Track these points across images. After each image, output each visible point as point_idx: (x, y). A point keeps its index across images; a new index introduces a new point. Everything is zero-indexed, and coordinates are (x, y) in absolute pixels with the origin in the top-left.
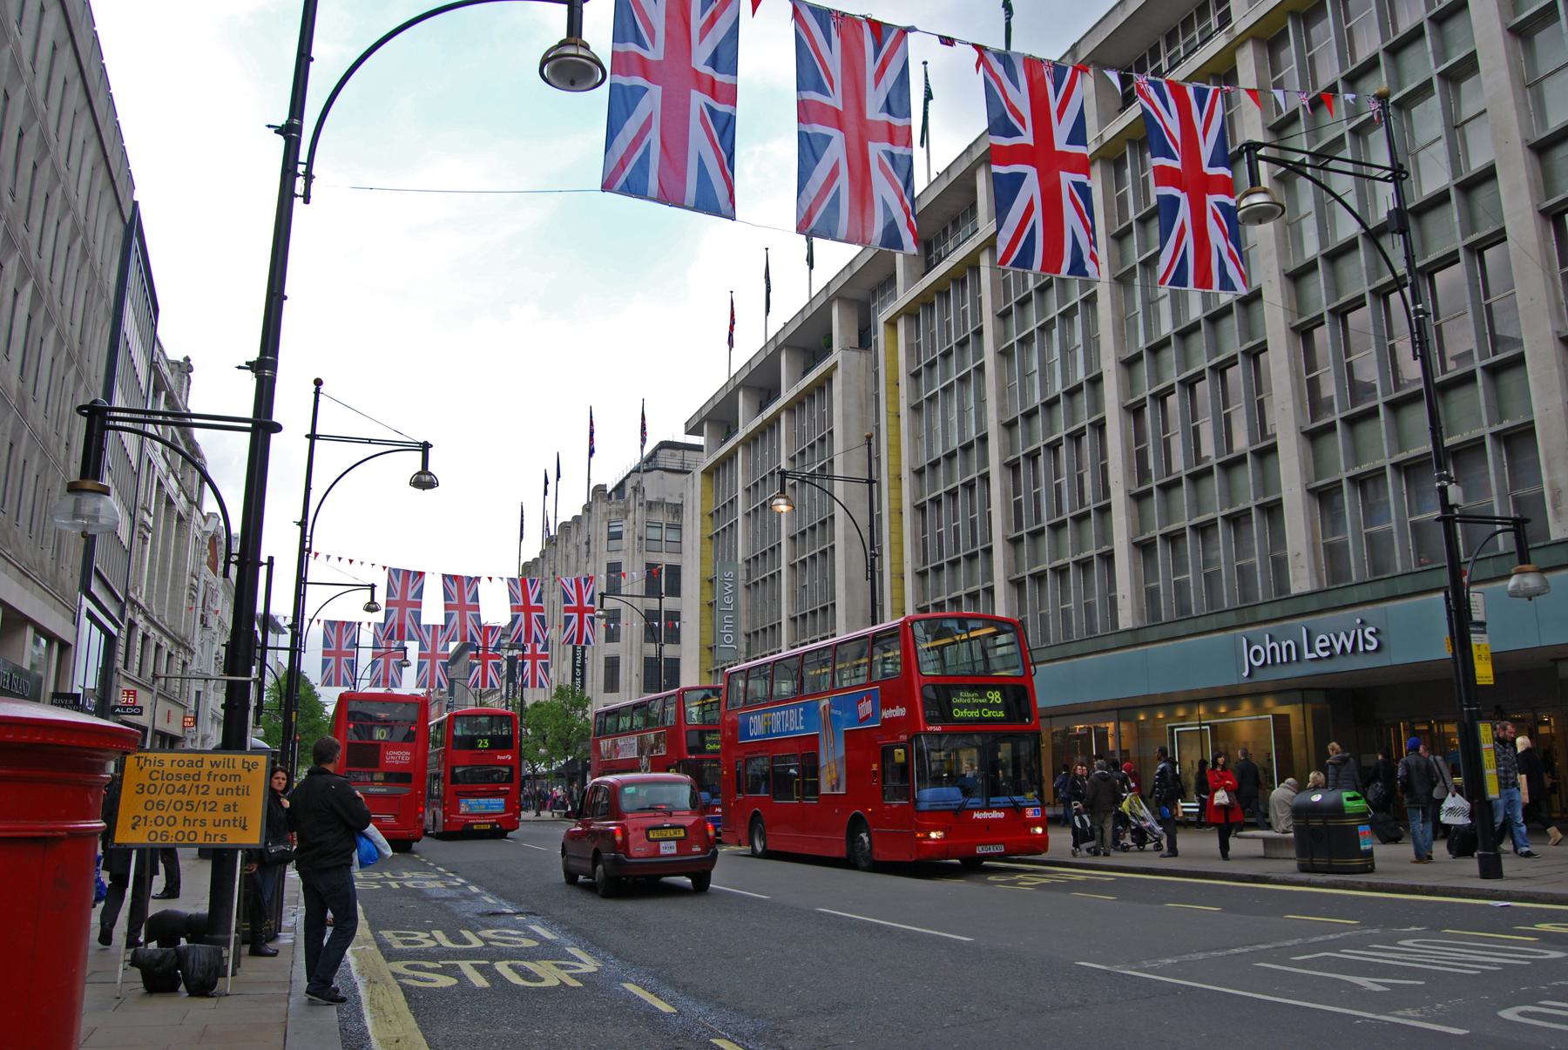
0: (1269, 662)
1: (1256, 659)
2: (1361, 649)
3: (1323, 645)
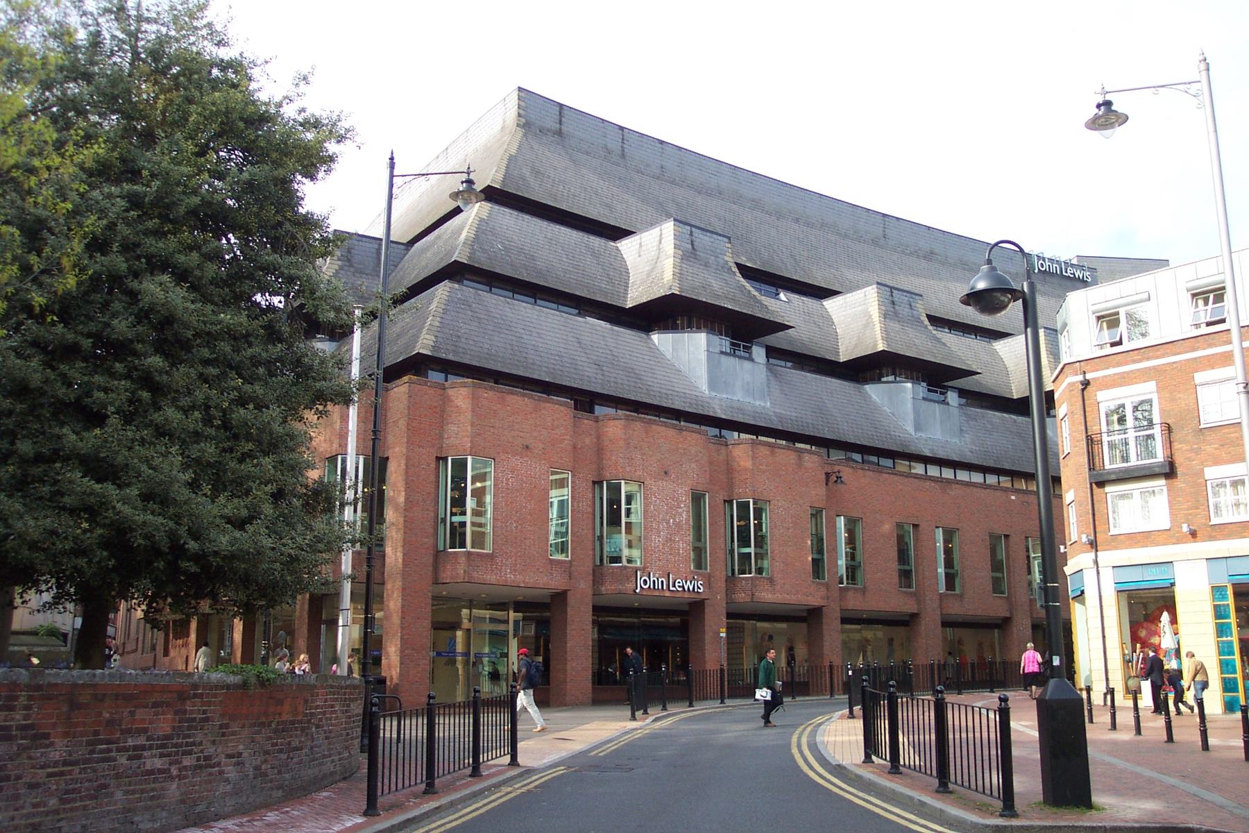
0: (652, 587)
1: (645, 581)
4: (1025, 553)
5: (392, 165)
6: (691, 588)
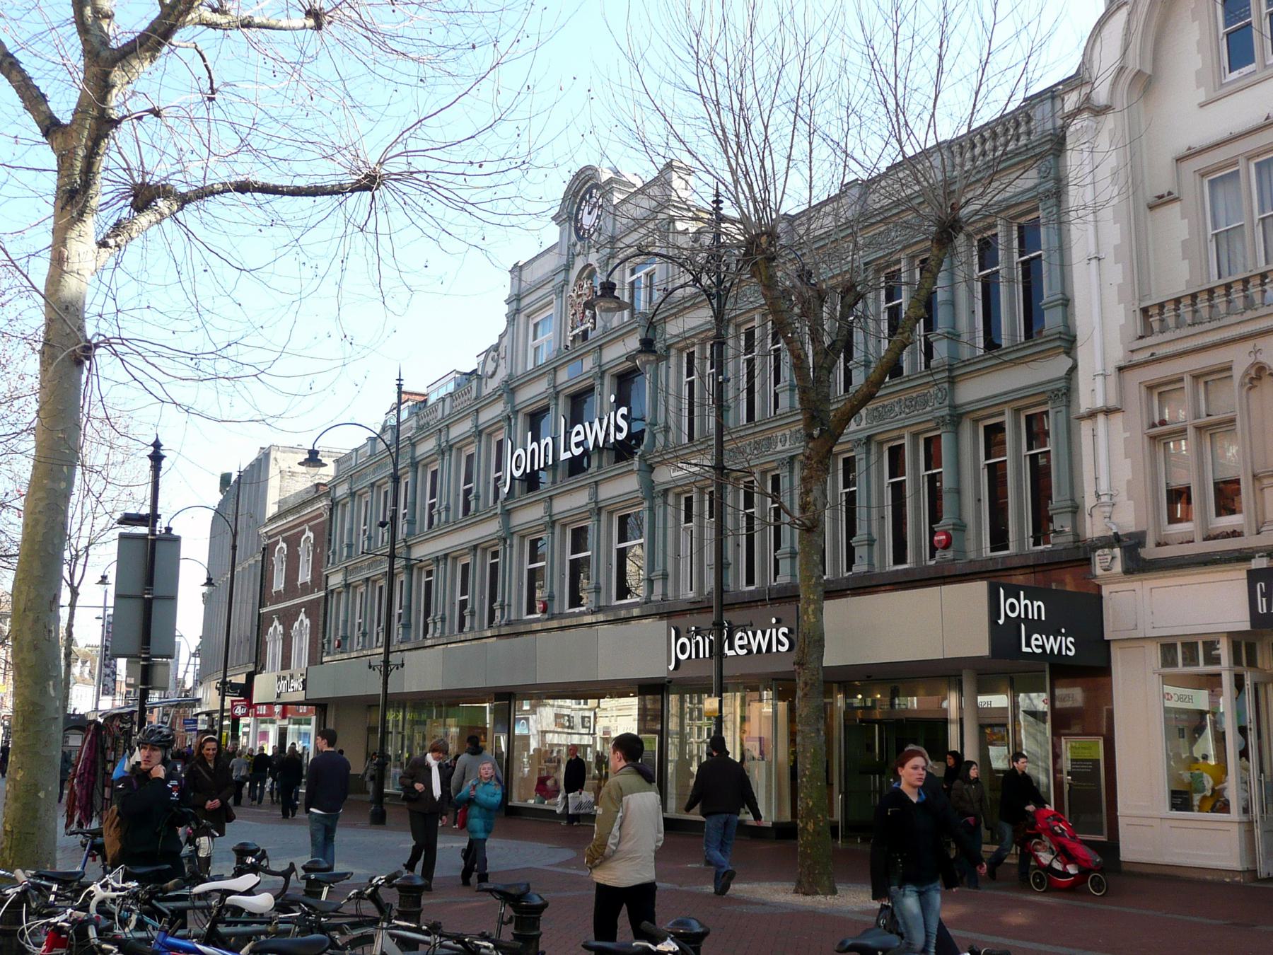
0: (693, 656)
2: (774, 650)
4: (203, 64)
5: (399, 386)
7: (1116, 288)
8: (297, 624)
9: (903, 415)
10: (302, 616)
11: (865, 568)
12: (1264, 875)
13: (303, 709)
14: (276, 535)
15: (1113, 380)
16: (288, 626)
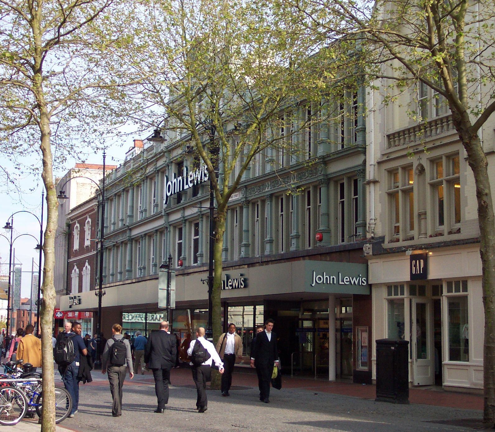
1: (320, 278)
3: (347, 280)
6: (356, 283)
7: (378, 125)
8: (84, 268)
9: (257, 193)
10: (87, 264)
11: (294, 249)
12: (416, 384)
13: (87, 314)
14: (74, 219)
15: (376, 166)
16: (81, 270)
